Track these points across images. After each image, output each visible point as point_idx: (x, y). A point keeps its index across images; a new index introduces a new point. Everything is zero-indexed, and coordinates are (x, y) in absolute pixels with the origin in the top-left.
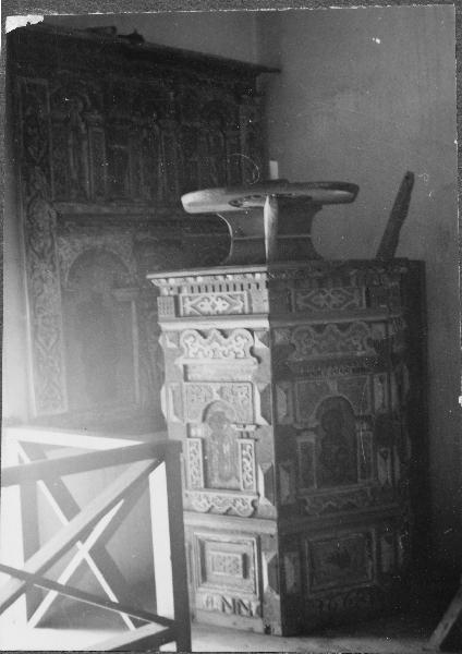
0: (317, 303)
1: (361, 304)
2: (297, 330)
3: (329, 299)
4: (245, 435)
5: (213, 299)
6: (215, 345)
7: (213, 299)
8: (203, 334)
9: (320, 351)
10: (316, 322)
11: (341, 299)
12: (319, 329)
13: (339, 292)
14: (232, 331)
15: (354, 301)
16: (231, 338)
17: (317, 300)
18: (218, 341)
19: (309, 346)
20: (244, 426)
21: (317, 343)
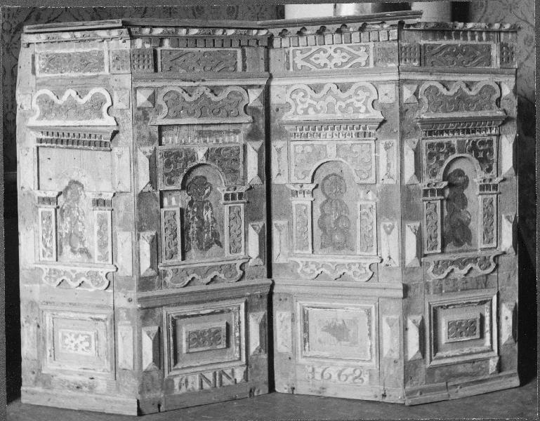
0: (317, 62)
5: (331, 51)
8: (316, 89)
9: (316, 110)
16: (351, 91)
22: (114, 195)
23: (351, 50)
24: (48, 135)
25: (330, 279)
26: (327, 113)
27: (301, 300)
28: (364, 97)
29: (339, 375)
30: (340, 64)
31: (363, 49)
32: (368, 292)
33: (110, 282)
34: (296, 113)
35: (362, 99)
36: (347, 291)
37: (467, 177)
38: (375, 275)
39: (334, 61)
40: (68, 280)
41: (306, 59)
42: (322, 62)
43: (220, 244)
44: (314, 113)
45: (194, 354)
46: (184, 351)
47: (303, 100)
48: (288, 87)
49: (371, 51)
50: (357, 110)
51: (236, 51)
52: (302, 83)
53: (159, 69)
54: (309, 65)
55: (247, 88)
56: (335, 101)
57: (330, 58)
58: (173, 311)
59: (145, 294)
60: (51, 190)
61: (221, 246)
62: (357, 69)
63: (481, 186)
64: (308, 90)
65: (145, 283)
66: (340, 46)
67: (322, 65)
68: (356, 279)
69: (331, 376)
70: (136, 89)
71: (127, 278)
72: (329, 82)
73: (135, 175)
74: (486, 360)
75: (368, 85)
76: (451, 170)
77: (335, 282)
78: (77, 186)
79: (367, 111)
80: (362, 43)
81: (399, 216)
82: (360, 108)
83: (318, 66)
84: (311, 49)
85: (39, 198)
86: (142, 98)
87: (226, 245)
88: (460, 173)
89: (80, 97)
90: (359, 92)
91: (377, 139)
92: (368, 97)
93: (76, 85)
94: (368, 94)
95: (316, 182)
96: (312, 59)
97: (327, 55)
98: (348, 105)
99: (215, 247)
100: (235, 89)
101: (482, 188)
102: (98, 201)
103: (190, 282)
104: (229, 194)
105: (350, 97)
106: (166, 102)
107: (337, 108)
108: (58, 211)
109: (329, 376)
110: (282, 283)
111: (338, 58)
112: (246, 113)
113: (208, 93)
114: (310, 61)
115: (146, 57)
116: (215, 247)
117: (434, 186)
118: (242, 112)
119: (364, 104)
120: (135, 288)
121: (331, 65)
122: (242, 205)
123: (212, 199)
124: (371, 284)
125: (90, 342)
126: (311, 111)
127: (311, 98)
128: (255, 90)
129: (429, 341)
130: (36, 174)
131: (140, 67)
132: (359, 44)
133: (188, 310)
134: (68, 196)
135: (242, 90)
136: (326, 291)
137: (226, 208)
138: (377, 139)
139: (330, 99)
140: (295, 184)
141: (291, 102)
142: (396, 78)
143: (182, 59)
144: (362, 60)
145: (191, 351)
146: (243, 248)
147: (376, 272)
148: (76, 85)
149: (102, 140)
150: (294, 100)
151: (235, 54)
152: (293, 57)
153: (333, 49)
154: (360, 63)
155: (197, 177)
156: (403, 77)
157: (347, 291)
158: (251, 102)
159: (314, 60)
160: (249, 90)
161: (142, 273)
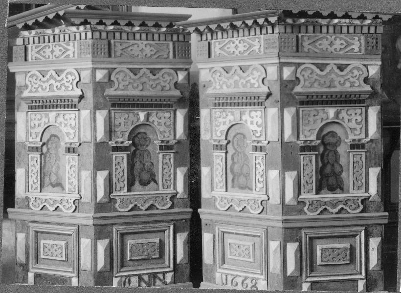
0: (229, 50)
1: (360, 51)
2: (303, 67)
3: (236, 47)
4: (71, 150)
5: (237, 42)
6: (52, 81)
7: (237, 42)
8: (227, 70)
9: (228, 87)
10: (224, 65)
11: (245, 46)
12: (134, 71)
13: (244, 41)
14: (231, 67)
15: (353, 47)
16: (63, 76)
17: (228, 48)
18: (238, 75)
19: (37, 86)
20: (219, 142)
21: (227, 81)
22: (80, 144)
23: (250, 41)
24: (36, 103)
25: (141, 210)
26: (234, 88)
27: (219, 225)
28: (257, 76)
29: (242, 283)
30: (242, 51)
31: (357, 38)
32: (259, 222)
33: (264, 208)
34: (215, 88)
35: (256, 78)
36: (248, 221)
37: (340, 138)
38: (265, 209)
39: (239, 49)
40: (48, 206)
41: (38, 52)
42: (232, 50)
43: (155, 182)
44: (226, 88)
45: (342, 266)
46: (128, 259)
47: (35, 82)
48: (210, 69)
49: (262, 42)
50: (252, 85)
51: (169, 44)
52: (218, 66)
53: (113, 55)
54: (223, 52)
55: (176, 70)
56: (239, 78)
57: (236, 47)
58: (313, 233)
59: (99, 215)
60: (36, 141)
61: (157, 184)
62: (253, 56)
63: (160, 146)
64: (128, 71)
65: (100, 207)
66: (243, 38)
67: (232, 52)
68: (252, 211)
69: (237, 283)
70: (95, 69)
71: (275, 205)
72: (236, 65)
73: (94, 128)
74: (357, 280)
75: (362, 67)
76: (325, 132)
77: (239, 213)
78: (56, 138)
79: (73, 89)
80: (257, 36)
81: (92, 167)
82: (254, 84)
83: (229, 53)
84: (225, 41)
85: (29, 147)
86: (100, 75)
87: (160, 182)
88: (333, 134)
89: (58, 75)
90: (165, 76)
91: (266, 107)
92: (259, 76)
93: (58, 66)
94: (171, 78)
95: (43, 141)
96: (226, 48)
97: (235, 45)
98: (247, 82)
99: (152, 183)
100: (168, 71)
101: (161, 148)
102: (69, 149)
103: (229, 207)
104: (163, 146)
105: (248, 76)
106: (117, 79)
107: (240, 84)
108: (43, 156)
109: (246, 285)
110: (204, 213)
111: (241, 48)
112: (77, 87)
113: (54, 73)
114: (224, 50)
115: (103, 46)
116: (152, 183)
117: (310, 143)
118: (173, 87)
119: (258, 81)
120: (93, 211)
121: (237, 52)
122: (172, 155)
123: (150, 148)
124: (262, 216)
125: (62, 250)
126: (224, 87)
127: (317, 75)
128: (182, 72)
129: (307, 261)
130: (28, 127)
131: (99, 53)
132: (255, 36)
133: (132, 228)
134: (49, 146)
135: (172, 72)
136: (235, 220)
137: (161, 156)
138: (266, 107)
139: (236, 78)
140: (215, 141)
141: (212, 80)
142: (277, 61)
143: (131, 48)
144: (256, 48)
145: (133, 258)
146: (172, 186)
147: (265, 207)
148: (58, 66)
149: (73, 103)
150: (214, 78)
151: (168, 46)
152: (214, 48)
153: (238, 41)
154: (69, 55)
155: (139, 133)
156: (283, 60)
157: (248, 221)
158: (179, 81)
159: (318, 46)
160: (178, 72)
161: (98, 200)
